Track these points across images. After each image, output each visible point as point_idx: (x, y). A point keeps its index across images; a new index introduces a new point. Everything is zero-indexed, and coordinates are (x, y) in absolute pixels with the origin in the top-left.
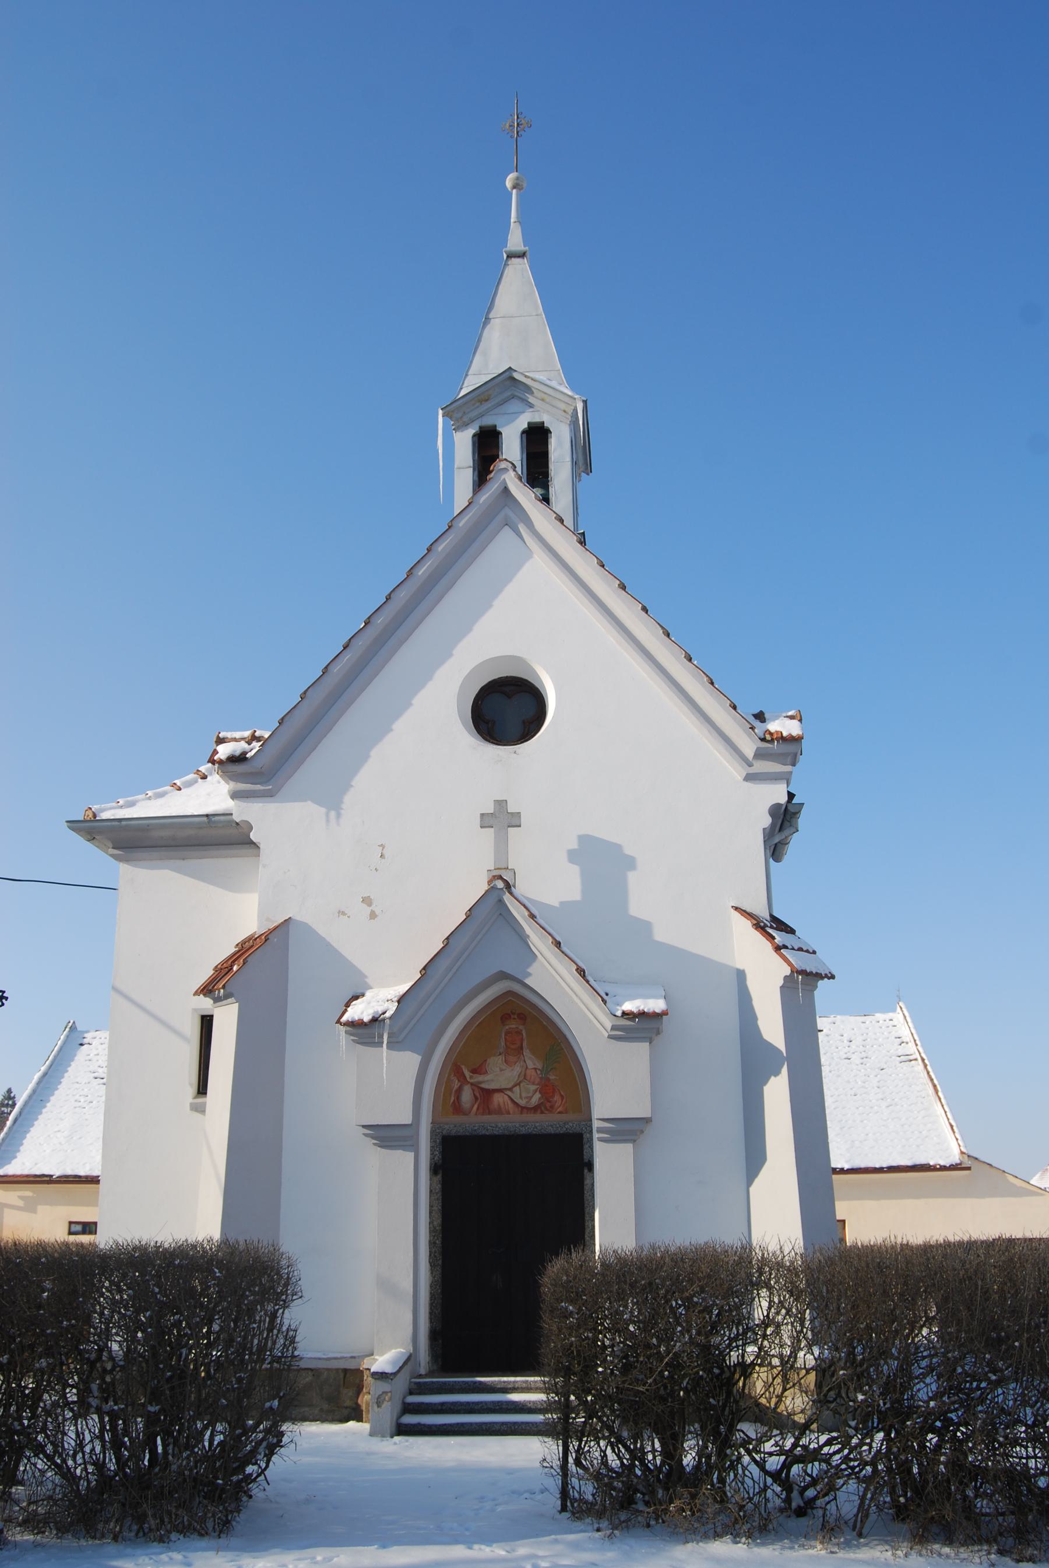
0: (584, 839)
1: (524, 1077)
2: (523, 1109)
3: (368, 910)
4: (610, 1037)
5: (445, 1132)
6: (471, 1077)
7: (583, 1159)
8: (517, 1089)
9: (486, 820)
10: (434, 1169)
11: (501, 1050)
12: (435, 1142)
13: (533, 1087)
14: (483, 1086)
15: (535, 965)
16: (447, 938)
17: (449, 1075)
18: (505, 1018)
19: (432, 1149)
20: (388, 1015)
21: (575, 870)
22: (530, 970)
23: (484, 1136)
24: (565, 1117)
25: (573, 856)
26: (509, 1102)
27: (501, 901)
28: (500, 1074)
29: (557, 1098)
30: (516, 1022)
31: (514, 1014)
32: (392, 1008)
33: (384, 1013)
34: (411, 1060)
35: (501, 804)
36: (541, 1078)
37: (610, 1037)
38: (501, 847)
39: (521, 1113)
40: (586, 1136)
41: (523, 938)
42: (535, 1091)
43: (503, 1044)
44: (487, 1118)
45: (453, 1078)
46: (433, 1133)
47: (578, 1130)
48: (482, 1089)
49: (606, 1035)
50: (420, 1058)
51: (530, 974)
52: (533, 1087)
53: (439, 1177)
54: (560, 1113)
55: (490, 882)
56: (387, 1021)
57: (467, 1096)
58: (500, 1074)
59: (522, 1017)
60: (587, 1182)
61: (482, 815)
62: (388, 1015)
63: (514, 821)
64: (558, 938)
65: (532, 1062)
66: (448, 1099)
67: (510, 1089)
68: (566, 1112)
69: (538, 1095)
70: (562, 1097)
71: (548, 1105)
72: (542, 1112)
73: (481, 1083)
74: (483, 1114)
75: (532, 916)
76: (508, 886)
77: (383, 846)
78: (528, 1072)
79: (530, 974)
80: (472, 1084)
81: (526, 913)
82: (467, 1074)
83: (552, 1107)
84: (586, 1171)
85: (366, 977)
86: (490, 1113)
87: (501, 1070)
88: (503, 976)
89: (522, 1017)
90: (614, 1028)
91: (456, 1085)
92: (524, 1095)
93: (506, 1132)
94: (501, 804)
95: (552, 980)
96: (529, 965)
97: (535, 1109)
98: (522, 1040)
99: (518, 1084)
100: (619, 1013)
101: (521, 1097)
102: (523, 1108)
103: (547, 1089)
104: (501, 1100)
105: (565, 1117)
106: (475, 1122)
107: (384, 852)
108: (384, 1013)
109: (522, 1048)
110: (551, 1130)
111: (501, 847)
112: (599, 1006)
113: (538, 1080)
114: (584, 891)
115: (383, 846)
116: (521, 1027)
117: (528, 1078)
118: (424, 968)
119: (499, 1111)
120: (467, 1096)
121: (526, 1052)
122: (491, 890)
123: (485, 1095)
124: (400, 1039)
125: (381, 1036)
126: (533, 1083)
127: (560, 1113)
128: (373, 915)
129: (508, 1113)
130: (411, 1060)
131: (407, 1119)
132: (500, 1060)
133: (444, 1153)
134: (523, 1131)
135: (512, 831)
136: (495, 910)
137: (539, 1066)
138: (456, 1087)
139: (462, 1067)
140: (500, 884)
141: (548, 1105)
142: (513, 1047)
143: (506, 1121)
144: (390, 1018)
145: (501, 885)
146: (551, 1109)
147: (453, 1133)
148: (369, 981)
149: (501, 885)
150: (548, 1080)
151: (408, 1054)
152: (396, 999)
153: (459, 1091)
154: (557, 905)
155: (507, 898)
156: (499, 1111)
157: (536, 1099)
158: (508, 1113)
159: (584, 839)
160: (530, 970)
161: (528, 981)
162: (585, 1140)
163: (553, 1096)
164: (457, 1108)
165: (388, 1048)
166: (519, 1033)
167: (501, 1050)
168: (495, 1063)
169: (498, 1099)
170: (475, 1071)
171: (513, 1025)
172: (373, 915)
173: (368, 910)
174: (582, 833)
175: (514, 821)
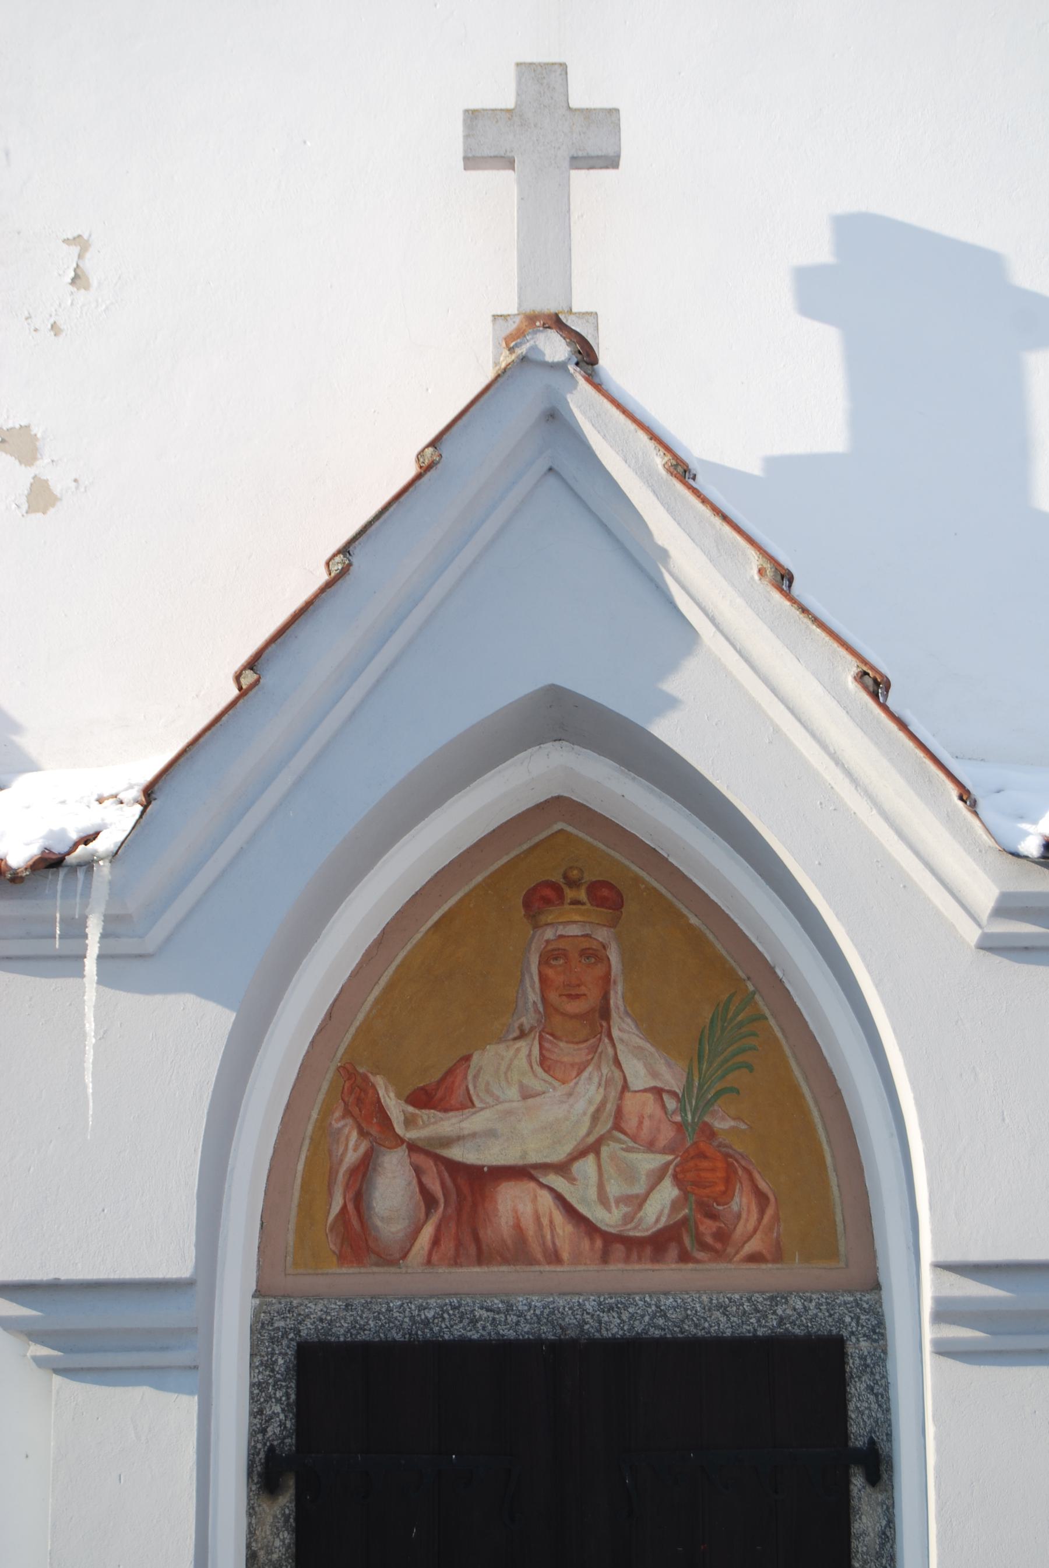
0: (854, 231)
1: (614, 1123)
2: (612, 1244)
3: (24, 476)
4: (990, 945)
5: (307, 1330)
6: (409, 1122)
7: (844, 1434)
8: (587, 1167)
9: (488, 142)
10: (267, 1472)
11: (528, 1020)
12: (270, 1365)
13: (648, 1162)
14: (456, 1153)
15: (692, 669)
16: (345, 550)
17: (326, 1113)
18: (541, 899)
19: (259, 1393)
20: (103, 845)
21: (824, 342)
22: (672, 686)
23: (463, 1347)
24: (769, 1277)
25: (814, 293)
26: (559, 1217)
27: (555, 418)
28: (522, 1111)
29: (741, 1202)
30: (591, 913)
31: (574, 884)
32: (118, 824)
33: (87, 840)
34: (193, 1028)
35: (543, 78)
36: (680, 1127)
37: (990, 945)
38: (546, 234)
39: (605, 1258)
40: (858, 1348)
41: (642, 564)
42: (659, 1176)
43: (533, 996)
44: (476, 1272)
45: (339, 1122)
46: (262, 1331)
47: (823, 1325)
48: (454, 1168)
49: (972, 934)
50: (232, 1016)
51: (671, 703)
52: (648, 1162)
53: (286, 1501)
54: (755, 1258)
55: (512, 341)
56: (104, 869)
57: (393, 1191)
58: (522, 1111)
59: (607, 897)
60: (865, 1523)
61: (472, 116)
62: (103, 845)
63: (595, 144)
64: (786, 561)
65: (643, 1066)
66: (320, 1205)
67: (562, 1168)
68: (778, 1255)
69: (667, 1192)
70: (762, 1199)
71: (708, 1227)
72: (685, 1257)
73: (448, 1142)
74: (456, 1262)
75: (682, 470)
76: (586, 356)
77: (81, 243)
78: (631, 1104)
79: (671, 703)
80: (413, 1147)
81: (659, 461)
82: (395, 1107)
83: (723, 1236)
84: (858, 1482)
85: (16, 727)
86: (481, 1259)
87: (526, 1095)
88: (562, 716)
89: (607, 897)
90: (1004, 909)
91: (351, 1149)
92: (614, 1189)
93: (548, 1333)
94: (543, 78)
95: (765, 728)
96: (670, 666)
97: (659, 1244)
98: (606, 980)
99: (594, 1148)
100: (1032, 847)
101: (603, 1199)
102: (610, 1240)
103: (703, 1168)
104: (526, 1209)
105: (769, 1277)
106: (424, 1290)
107: (87, 264)
108: (87, 840)
109: (605, 1012)
110: (722, 1325)
111: (546, 234)
112: (949, 820)
113: (667, 1134)
114: (859, 418)
115: (81, 243)
116: (602, 935)
117: (631, 1123)
118: (252, 664)
119: (518, 1251)
120: (393, 1191)
121: (624, 1030)
122: (518, 369)
123: (464, 1190)
124: (150, 944)
125: (76, 930)
126: (650, 1146)
127: (755, 1258)
128: (40, 497)
129: (554, 1257)
130: (193, 1028)
131: (176, 1262)
132: (526, 1051)
133: (304, 1409)
134: (614, 1327)
135: (584, 182)
136: (535, 432)
137: (672, 1079)
138: (351, 1157)
139: (374, 1081)
140: (555, 348)
141: (708, 1227)
142: (573, 1007)
143: (542, 1287)
144: (114, 856)
145: (552, 356)
146: (720, 1245)
147: (340, 1332)
148: (28, 743)
149: (552, 356)
150: (711, 1133)
151: (189, 1001)
152: (136, 793)
153: (364, 1171)
154: (755, 468)
155: (581, 402)
156: (518, 1251)
157: (661, 1205)
158: (554, 1257)
159: (854, 231)
160: (672, 686)
161: (668, 731)
162: (853, 1364)
163: (727, 1194)
164: (356, 1239)
165: (103, 979)
166: (595, 955)
167: (528, 1020)
168: (504, 1068)
169: (514, 1205)
170: (424, 1098)
171: (570, 925)
172: (40, 497)
173: (24, 476)
174: (847, 206)
175: (595, 144)
